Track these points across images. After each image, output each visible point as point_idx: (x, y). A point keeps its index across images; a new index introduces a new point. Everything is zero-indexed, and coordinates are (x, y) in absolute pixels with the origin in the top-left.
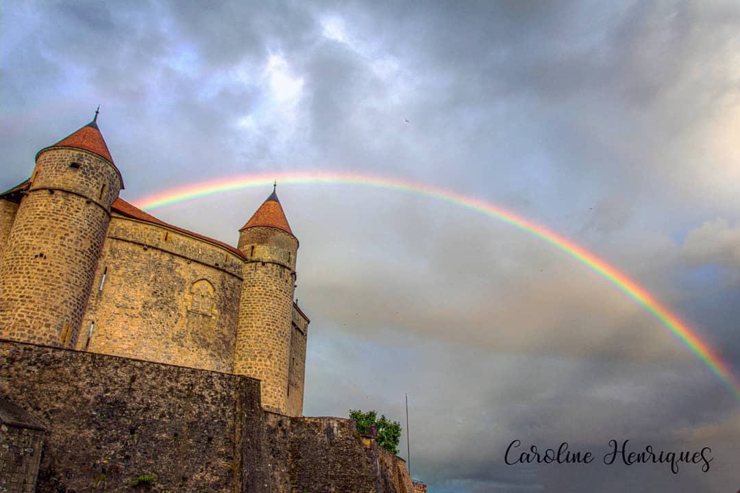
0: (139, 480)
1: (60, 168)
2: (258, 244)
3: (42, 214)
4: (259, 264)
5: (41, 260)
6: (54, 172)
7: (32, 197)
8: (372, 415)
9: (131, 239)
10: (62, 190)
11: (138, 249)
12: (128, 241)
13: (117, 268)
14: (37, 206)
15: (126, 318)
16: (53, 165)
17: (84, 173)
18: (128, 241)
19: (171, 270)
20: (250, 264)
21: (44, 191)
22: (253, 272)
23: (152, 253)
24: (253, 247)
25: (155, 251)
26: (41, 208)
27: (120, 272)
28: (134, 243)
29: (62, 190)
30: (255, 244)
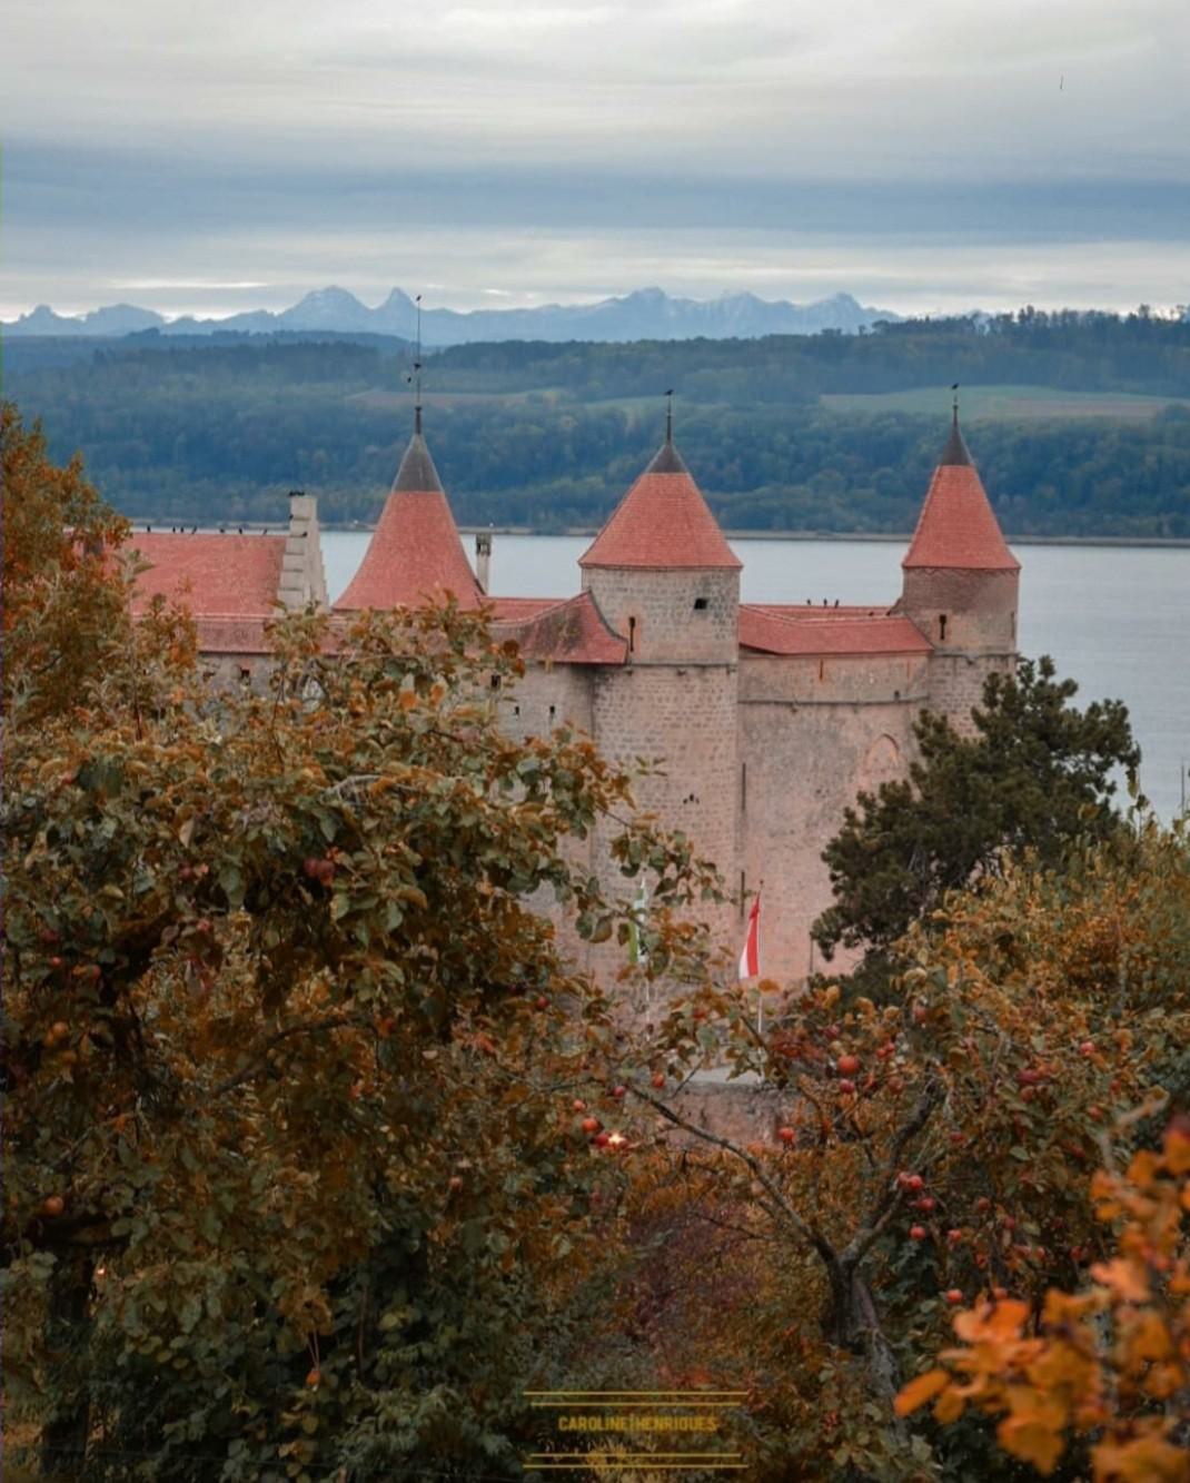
0: (46, 1383)
1: (680, 614)
2: (955, 612)
3: (674, 718)
4: (962, 663)
5: (692, 806)
6: (671, 626)
7: (643, 680)
8: (839, 331)
9: (770, 696)
10: (696, 666)
11: (784, 712)
12: (768, 703)
13: (760, 761)
14: (660, 700)
15: (787, 853)
16: (666, 609)
17: (716, 616)
18: (768, 703)
19: (834, 737)
20: (941, 661)
21: (666, 670)
22: (949, 678)
23: (805, 715)
24: (943, 619)
25: (809, 709)
26: (670, 706)
27: (765, 766)
28: (777, 703)
29: (696, 666)
30: (948, 613)
